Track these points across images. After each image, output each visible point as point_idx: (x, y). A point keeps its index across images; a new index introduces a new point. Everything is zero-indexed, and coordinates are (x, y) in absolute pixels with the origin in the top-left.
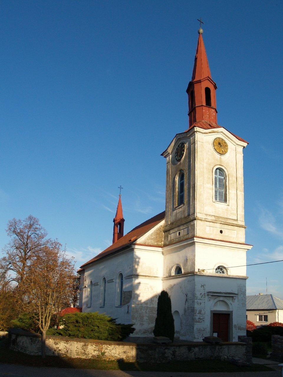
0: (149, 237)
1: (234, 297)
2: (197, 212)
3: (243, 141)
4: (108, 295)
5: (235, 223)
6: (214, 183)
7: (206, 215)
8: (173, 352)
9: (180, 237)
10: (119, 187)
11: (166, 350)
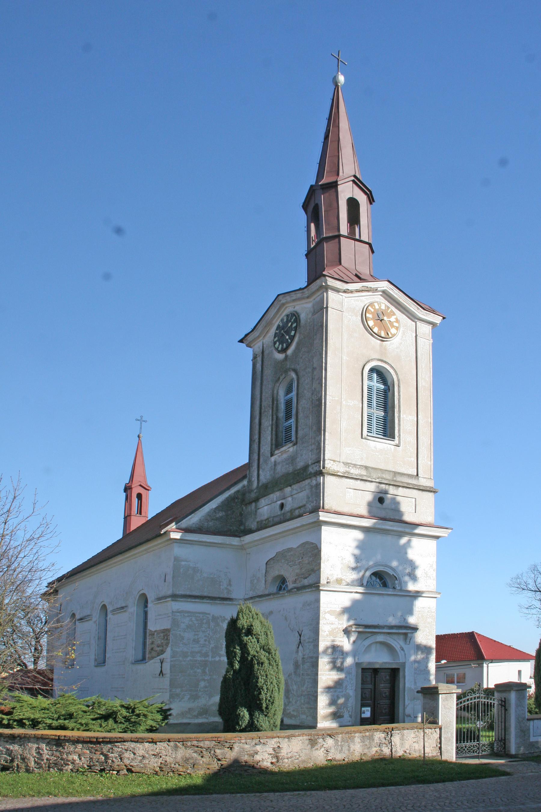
0: (210, 516)
1: (409, 635)
2: (326, 458)
3: (433, 312)
4: (114, 640)
5: (414, 482)
6: (367, 402)
7: (346, 464)
8: (274, 749)
9: (284, 514)
10: (137, 420)
11: (258, 748)
